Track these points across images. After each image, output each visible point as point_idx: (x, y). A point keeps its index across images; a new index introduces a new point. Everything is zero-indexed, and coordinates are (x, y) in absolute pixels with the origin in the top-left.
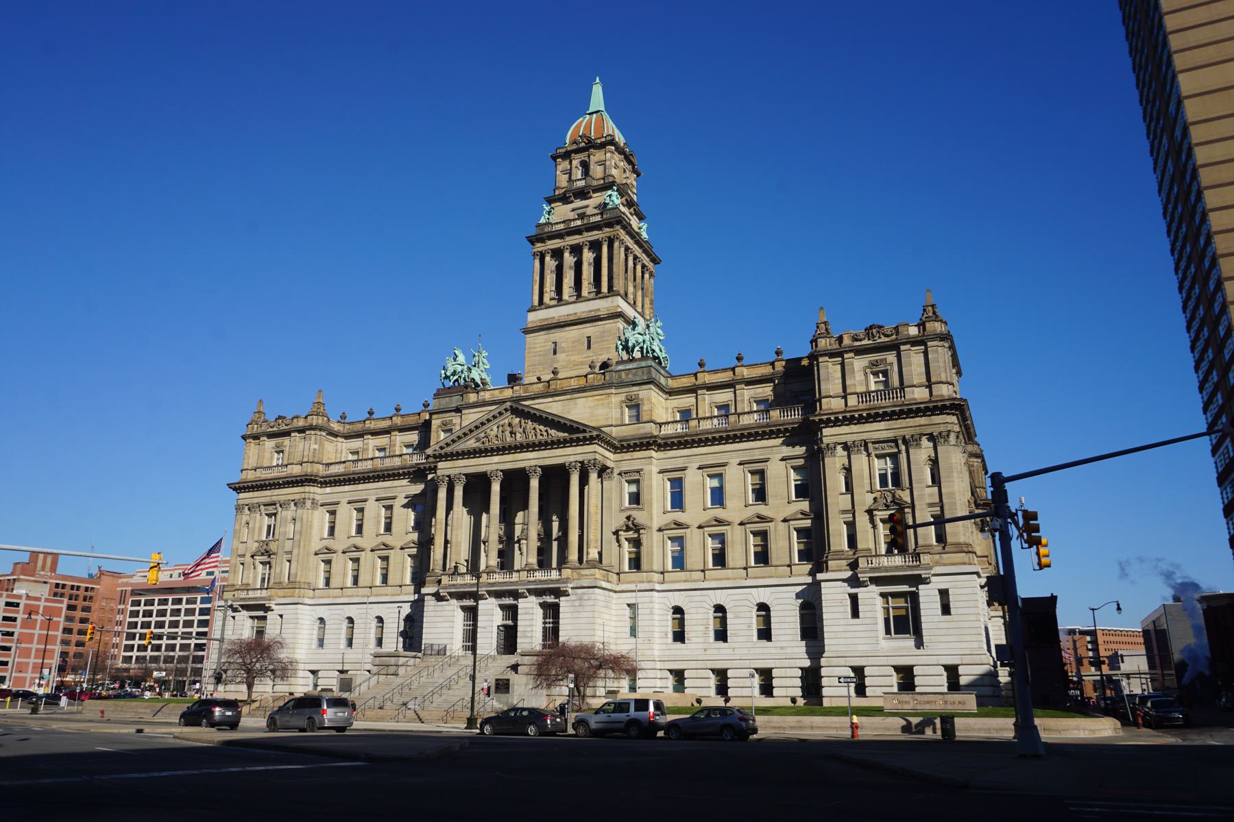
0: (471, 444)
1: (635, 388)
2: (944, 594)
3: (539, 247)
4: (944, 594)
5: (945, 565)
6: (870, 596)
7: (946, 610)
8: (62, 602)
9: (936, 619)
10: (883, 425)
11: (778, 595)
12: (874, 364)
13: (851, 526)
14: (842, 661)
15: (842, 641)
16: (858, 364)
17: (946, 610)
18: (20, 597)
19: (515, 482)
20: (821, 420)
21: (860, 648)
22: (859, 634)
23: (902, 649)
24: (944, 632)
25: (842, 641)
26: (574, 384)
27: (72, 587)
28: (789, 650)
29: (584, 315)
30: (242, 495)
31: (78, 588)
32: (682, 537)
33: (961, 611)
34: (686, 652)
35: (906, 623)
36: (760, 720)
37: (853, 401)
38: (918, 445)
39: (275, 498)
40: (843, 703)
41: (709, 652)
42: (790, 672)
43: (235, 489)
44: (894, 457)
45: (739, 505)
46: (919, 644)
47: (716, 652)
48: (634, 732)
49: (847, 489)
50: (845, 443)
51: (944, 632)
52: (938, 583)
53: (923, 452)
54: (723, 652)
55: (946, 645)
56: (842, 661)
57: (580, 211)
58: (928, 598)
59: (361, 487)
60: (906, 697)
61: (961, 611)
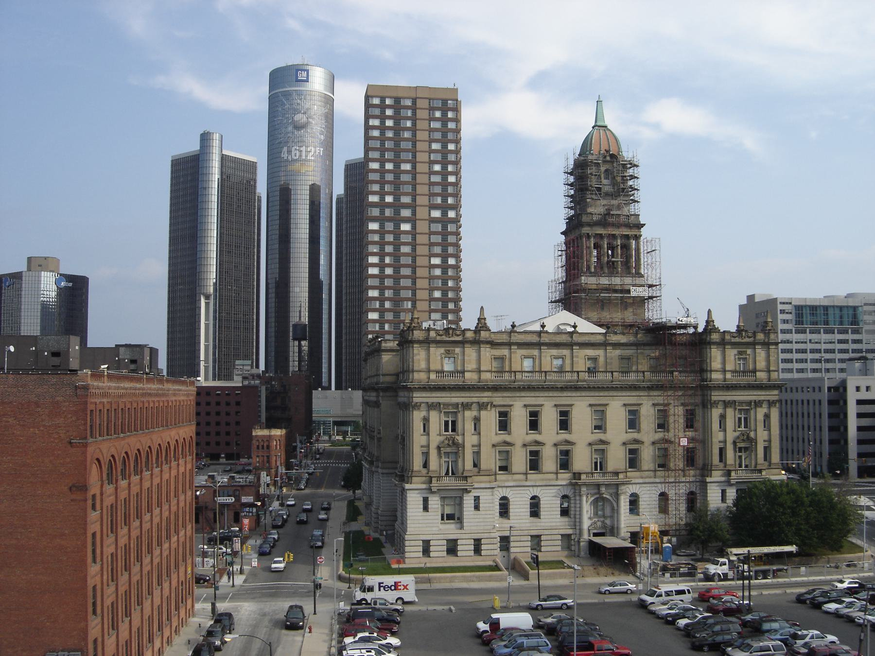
2: (477, 499)
4: (477, 499)
6: (435, 502)
7: (477, 507)
9: (420, 514)
13: (426, 455)
16: (731, 353)
17: (477, 507)
23: (450, 530)
32: (603, 450)
35: (454, 517)
37: (729, 376)
38: (761, 406)
42: (464, 553)
44: (747, 411)
45: (648, 432)
46: (462, 528)
48: (565, 606)
49: (424, 431)
50: (724, 401)
53: (761, 412)
58: (468, 501)
60: (426, 560)
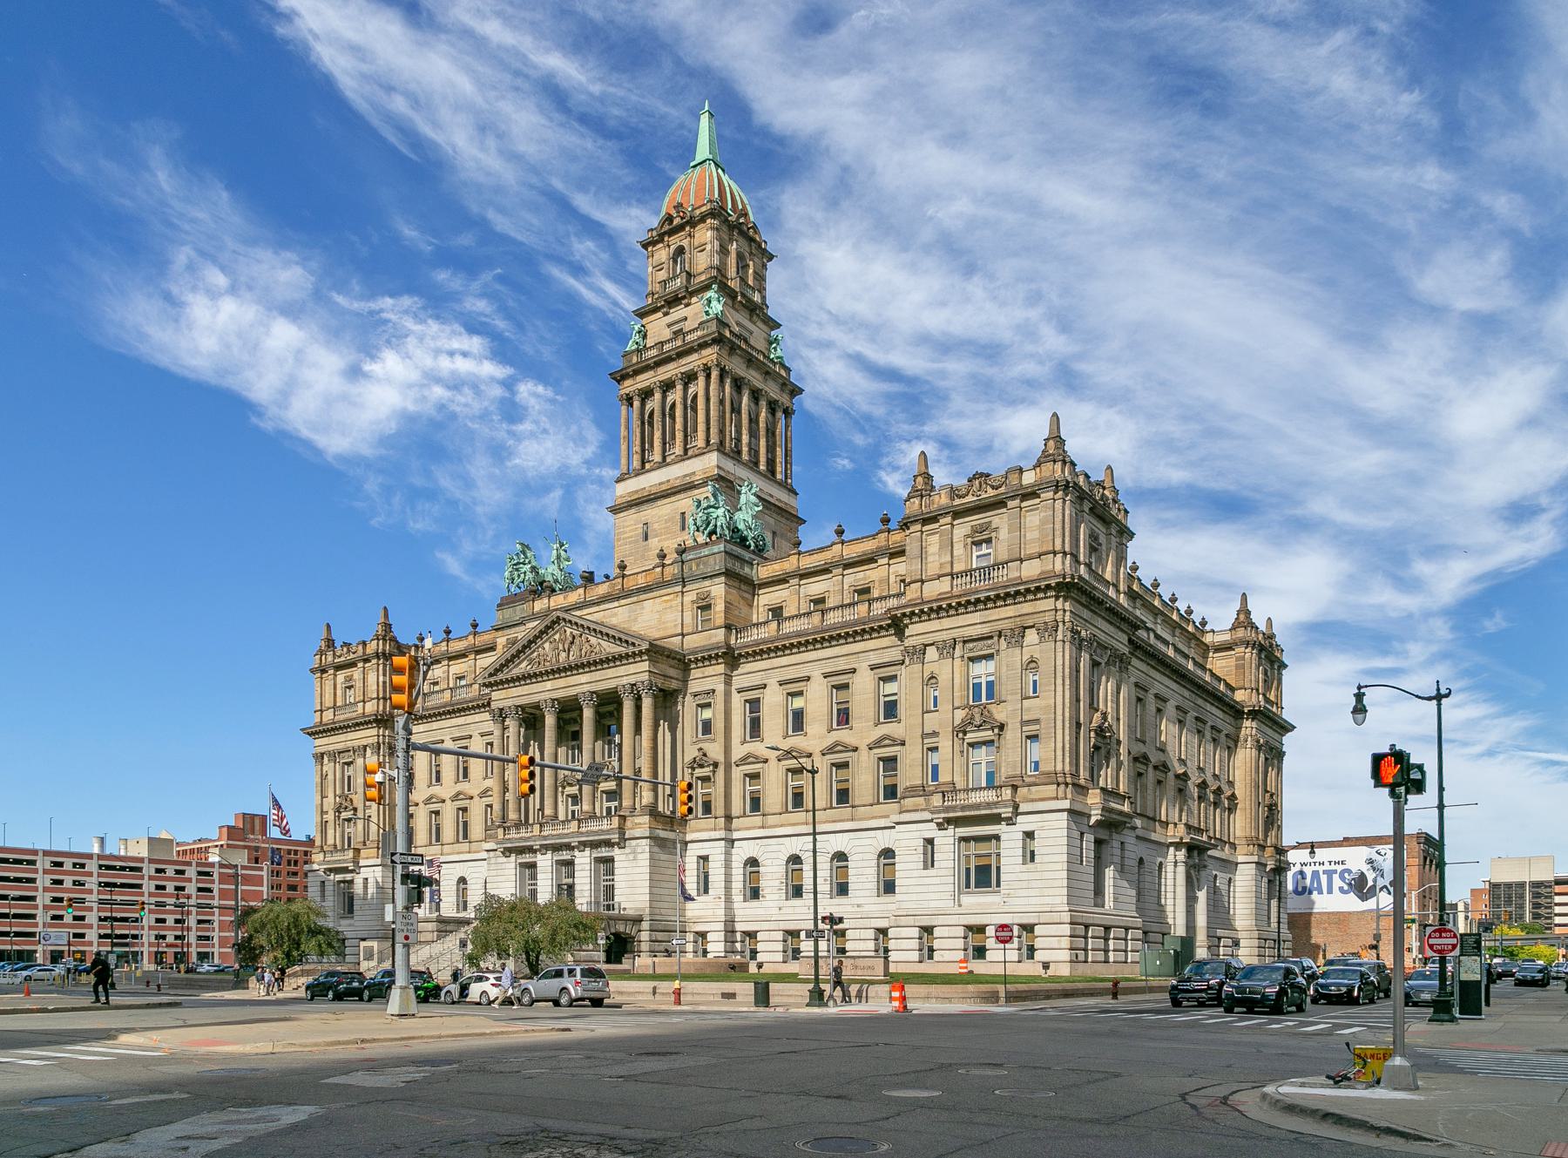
0: (523, 667)
1: (707, 583)
3: (630, 386)
5: (1033, 801)
8: (261, 869)
10: (976, 617)
11: (857, 842)
12: (976, 530)
14: (910, 920)
15: (914, 897)
18: (212, 865)
19: (568, 711)
20: (904, 615)
21: (933, 904)
22: (932, 888)
24: (1024, 884)
25: (914, 897)
26: (641, 581)
27: (289, 852)
28: (866, 908)
29: (678, 483)
30: (318, 742)
31: (296, 852)
33: (1046, 859)
34: (761, 911)
36: (88, 1001)
39: (349, 744)
40: (954, 969)
41: (866, 908)
43: (310, 734)
47: (790, 910)
51: (1024, 884)
52: (1024, 823)
54: (798, 910)
55: (1025, 901)
56: (910, 920)
57: (676, 328)
59: (435, 725)
61: (1046, 859)
